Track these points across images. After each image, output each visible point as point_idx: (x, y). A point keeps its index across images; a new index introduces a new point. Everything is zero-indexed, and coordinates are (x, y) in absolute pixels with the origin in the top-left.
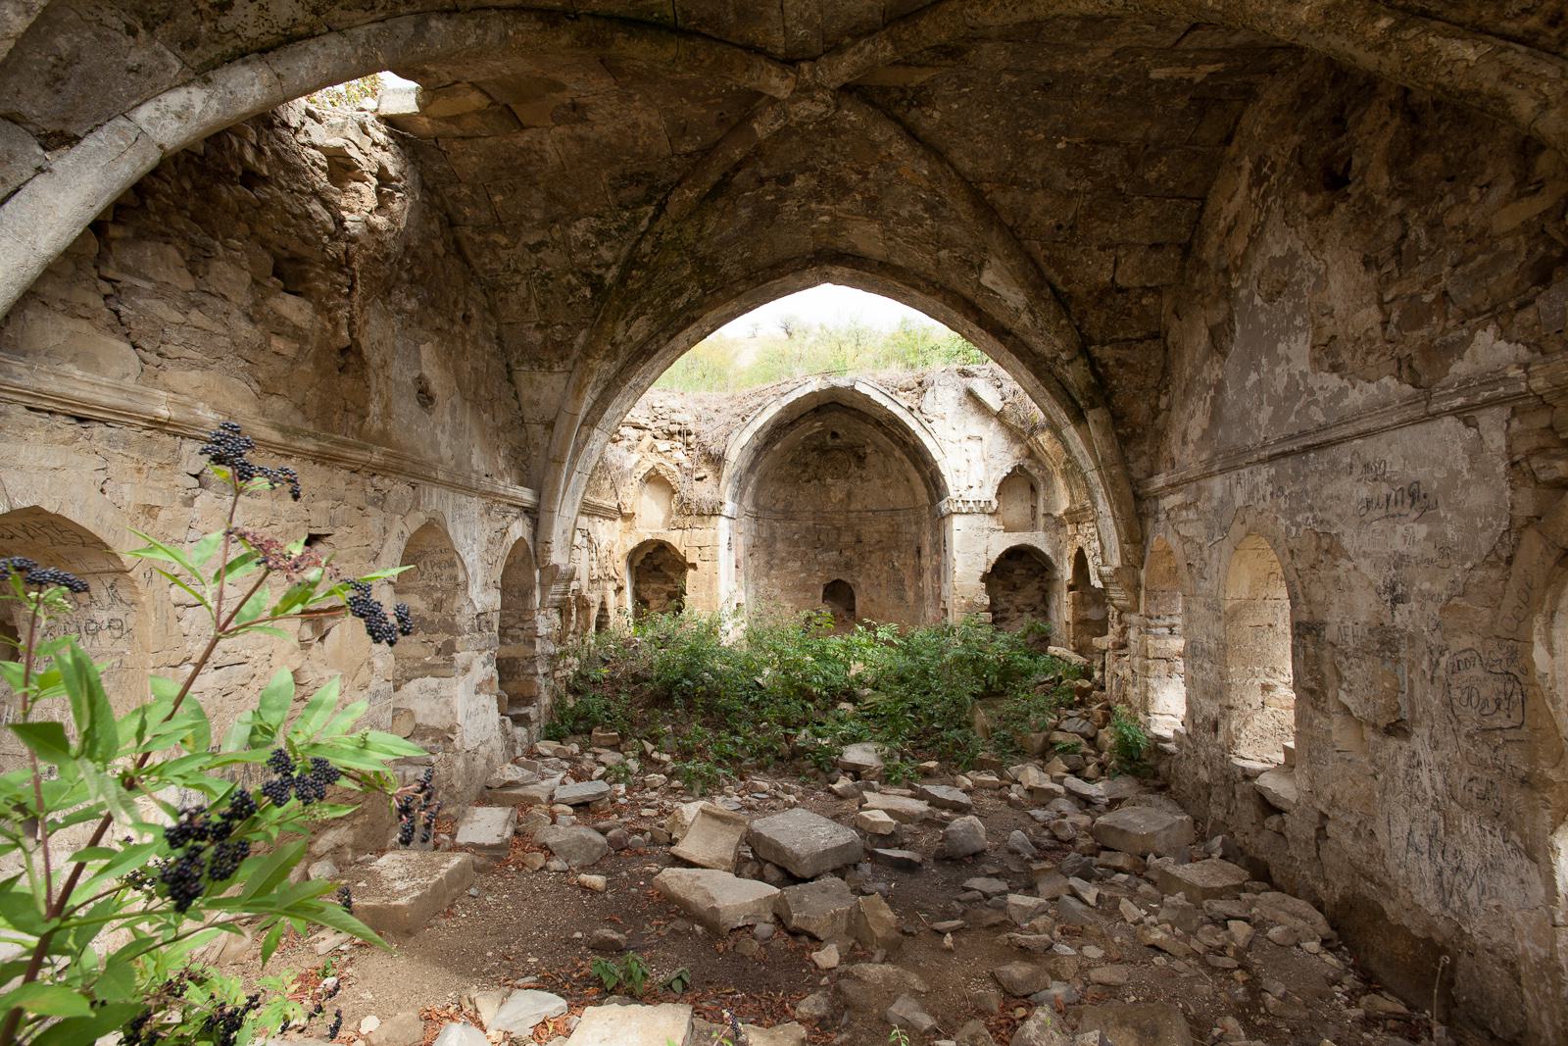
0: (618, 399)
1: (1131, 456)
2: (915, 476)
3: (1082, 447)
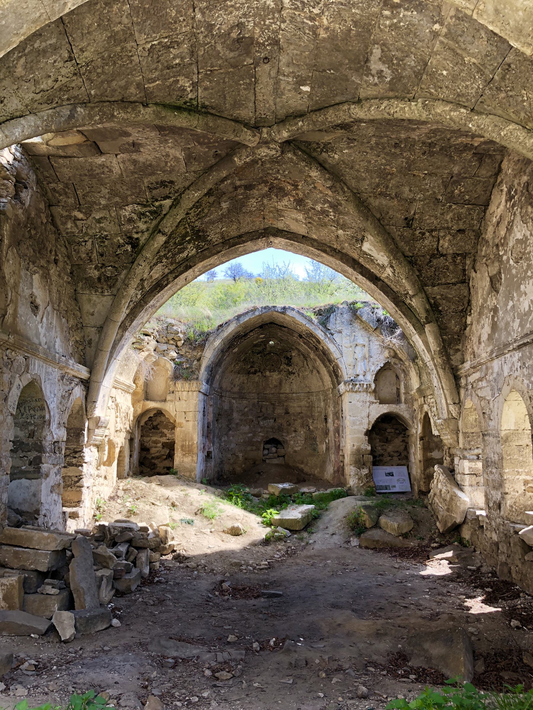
0: (142, 314)
1: (451, 352)
2: (324, 371)
3: (423, 347)
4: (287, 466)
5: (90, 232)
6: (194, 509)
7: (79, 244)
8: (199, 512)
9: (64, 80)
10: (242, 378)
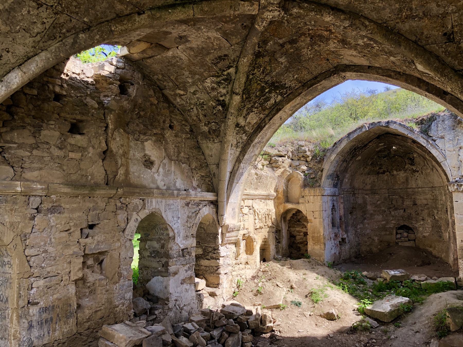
4: (417, 249)
5: (193, 102)
6: (306, 292)
7: (189, 111)
8: (310, 295)
9: (51, 21)
10: (372, 178)
